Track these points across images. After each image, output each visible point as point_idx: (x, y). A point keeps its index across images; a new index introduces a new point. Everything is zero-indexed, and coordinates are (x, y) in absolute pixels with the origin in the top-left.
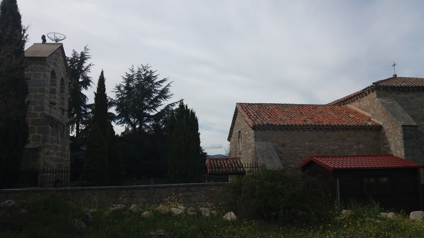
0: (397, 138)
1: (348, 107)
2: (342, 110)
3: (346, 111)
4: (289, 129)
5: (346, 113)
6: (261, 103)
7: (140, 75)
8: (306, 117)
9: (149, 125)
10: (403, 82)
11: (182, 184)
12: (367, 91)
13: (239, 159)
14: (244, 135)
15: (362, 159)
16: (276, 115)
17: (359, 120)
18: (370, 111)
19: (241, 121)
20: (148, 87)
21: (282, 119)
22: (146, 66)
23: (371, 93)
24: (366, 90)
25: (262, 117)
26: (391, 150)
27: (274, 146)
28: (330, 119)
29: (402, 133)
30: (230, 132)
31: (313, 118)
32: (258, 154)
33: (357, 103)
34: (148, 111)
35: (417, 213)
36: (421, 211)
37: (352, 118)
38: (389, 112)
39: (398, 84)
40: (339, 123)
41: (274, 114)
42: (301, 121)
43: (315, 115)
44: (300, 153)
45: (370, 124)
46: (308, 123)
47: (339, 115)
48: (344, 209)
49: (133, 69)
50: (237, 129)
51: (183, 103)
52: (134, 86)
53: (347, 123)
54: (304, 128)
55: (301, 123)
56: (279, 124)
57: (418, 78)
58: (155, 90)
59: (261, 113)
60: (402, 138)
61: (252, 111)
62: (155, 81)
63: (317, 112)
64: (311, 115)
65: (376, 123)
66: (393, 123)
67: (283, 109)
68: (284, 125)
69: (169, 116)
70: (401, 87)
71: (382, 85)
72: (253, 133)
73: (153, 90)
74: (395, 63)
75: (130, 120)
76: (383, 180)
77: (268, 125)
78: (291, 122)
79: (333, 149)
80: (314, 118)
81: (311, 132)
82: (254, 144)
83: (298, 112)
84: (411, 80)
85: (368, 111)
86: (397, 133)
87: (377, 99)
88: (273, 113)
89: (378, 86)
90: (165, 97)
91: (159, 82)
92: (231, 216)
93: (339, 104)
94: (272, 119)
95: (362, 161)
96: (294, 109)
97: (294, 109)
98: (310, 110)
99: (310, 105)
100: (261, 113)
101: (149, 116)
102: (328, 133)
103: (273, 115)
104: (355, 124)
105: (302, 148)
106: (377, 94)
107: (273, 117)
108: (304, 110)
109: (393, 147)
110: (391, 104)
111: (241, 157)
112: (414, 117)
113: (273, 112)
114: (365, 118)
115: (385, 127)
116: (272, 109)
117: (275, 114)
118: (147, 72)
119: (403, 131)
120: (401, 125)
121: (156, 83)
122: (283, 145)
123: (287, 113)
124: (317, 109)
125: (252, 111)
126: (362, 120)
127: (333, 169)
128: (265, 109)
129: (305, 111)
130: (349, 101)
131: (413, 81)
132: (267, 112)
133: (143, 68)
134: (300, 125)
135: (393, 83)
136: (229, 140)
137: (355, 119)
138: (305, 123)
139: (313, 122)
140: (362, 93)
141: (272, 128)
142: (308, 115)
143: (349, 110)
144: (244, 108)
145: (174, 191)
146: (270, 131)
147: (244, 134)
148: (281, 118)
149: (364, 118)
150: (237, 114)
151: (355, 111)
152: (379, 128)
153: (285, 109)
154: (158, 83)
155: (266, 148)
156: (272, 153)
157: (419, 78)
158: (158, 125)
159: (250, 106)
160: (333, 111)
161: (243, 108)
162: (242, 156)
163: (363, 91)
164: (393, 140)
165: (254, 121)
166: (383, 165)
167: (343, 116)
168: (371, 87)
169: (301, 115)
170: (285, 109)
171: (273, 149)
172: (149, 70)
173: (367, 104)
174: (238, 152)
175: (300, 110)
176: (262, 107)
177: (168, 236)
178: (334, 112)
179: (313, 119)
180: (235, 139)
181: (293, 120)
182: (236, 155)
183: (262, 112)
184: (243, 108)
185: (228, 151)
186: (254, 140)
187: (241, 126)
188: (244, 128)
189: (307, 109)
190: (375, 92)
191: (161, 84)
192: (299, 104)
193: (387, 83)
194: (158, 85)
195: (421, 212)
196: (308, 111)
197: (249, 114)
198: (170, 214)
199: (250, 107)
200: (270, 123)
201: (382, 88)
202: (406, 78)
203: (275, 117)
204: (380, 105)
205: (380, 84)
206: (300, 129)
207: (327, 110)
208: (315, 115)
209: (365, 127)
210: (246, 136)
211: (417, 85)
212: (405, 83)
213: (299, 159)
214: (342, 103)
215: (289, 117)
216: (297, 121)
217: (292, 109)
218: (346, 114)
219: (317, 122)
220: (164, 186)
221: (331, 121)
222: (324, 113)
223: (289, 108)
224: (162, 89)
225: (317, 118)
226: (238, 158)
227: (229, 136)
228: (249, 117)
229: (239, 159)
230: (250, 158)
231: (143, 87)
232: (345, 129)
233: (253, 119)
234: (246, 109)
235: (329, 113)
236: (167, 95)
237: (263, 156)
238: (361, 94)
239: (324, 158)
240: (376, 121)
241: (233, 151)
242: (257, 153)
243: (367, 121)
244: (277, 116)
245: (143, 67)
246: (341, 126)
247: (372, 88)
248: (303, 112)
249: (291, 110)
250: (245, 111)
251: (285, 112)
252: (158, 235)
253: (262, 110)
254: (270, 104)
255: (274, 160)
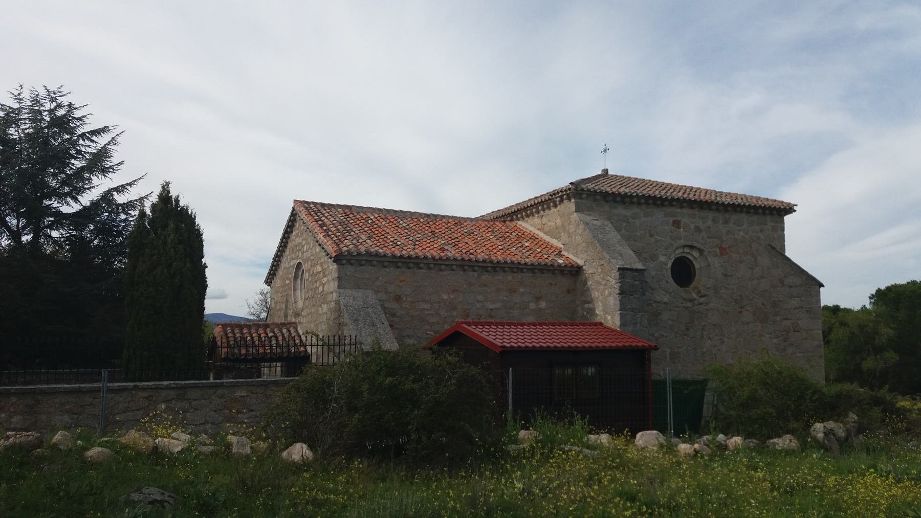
0: (608, 291)
1: (519, 227)
2: (508, 232)
3: (515, 234)
4: (411, 265)
5: (516, 239)
6: (351, 205)
7: (40, 112)
8: (443, 242)
9: (59, 238)
10: (621, 184)
11: (165, 383)
12: (558, 197)
13: (294, 325)
14: (311, 273)
15: (511, 329)
16: (383, 233)
17: (541, 254)
18: (560, 236)
19: (304, 242)
20: (61, 142)
21: (396, 243)
22: (55, 89)
23: (564, 201)
24: (557, 196)
25: (355, 236)
26: (597, 314)
27: (379, 300)
28: (488, 249)
29: (618, 283)
30: (273, 265)
31: (457, 245)
32: (344, 316)
33: (536, 220)
34: (56, 202)
35: (647, 434)
36: (653, 430)
37: (528, 248)
38: (596, 242)
39: (614, 187)
40: (506, 257)
41: (378, 231)
42: (435, 249)
43: (460, 238)
44: (429, 314)
45: (561, 261)
46: (447, 255)
47: (505, 241)
48: (521, 429)
49: (19, 94)
50: (293, 260)
51: (169, 192)
52: (20, 138)
53: (521, 258)
54: (441, 264)
55: (435, 254)
56: (392, 254)
57: (644, 180)
58: (79, 152)
59: (352, 227)
60: (618, 291)
61: (331, 221)
62: (79, 131)
63: (462, 232)
64: (453, 237)
65: (571, 261)
66: (602, 262)
67: (396, 220)
68: (401, 257)
69: (111, 217)
70: (619, 194)
71: (587, 187)
72: (334, 269)
73: (73, 152)
74: (608, 147)
75: (7, 222)
76: (587, 371)
77: (368, 253)
78: (415, 250)
79: (491, 309)
80: (459, 245)
81: (453, 272)
82: (335, 295)
83: (427, 230)
84: (633, 181)
85: (558, 236)
86: (608, 282)
87: (575, 214)
88: (375, 228)
89: (579, 189)
90: (105, 171)
91: (89, 134)
92: (299, 452)
93: (502, 219)
94: (376, 242)
95: (511, 335)
96: (419, 222)
97: (419, 222)
98: (450, 226)
99: (448, 216)
100: (352, 227)
101: (59, 215)
102: (485, 277)
103: (376, 232)
104: (534, 260)
105: (434, 304)
106: (577, 204)
107: (377, 238)
108: (437, 227)
109: (601, 308)
110: (600, 226)
111: (300, 323)
112: (638, 253)
113: (375, 226)
114: (551, 251)
115: (587, 270)
116: (374, 220)
117: (380, 230)
118: (60, 106)
119: (619, 279)
120: (618, 267)
121: (83, 136)
122: (398, 299)
123: (406, 231)
124: (462, 226)
125: (331, 221)
126: (546, 253)
127: (500, 350)
128: (358, 219)
129: (440, 230)
130: (522, 214)
131: (638, 185)
132: (364, 226)
133: (47, 95)
134: (433, 258)
135: (605, 186)
136: (268, 281)
137: (534, 252)
138: (442, 254)
139: (458, 253)
140: (548, 200)
141: (377, 261)
142: (447, 237)
143: (521, 231)
144: (313, 213)
145: (145, 398)
146: (373, 268)
147: (311, 271)
148: (395, 241)
149: (550, 250)
150: (293, 226)
151: (532, 234)
152: (575, 271)
153: (401, 222)
154: (87, 135)
155: (362, 304)
156: (375, 314)
157: (647, 180)
158: (81, 238)
159: (325, 210)
160: (492, 231)
161: (310, 213)
162: (301, 319)
163: (550, 197)
164: (600, 294)
165: (338, 245)
166: (561, 343)
167: (512, 243)
168: (566, 190)
169: (432, 236)
170: (401, 222)
171: (378, 307)
172: (65, 101)
173: (556, 223)
174: (292, 311)
175: (430, 227)
176: (353, 214)
177: (170, 502)
178: (494, 235)
179: (457, 247)
180: (285, 281)
181: (418, 246)
182: (286, 316)
183: (354, 224)
184: (310, 213)
185: (256, 307)
186: (337, 286)
187: (303, 253)
188: (312, 258)
189: (444, 224)
190: (573, 200)
191: (94, 138)
192: (428, 213)
193: (594, 185)
194: (86, 141)
195: (655, 432)
196: (447, 230)
197: (325, 228)
198: (157, 453)
199: (325, 212)
200: (374, 250)
201: (587, 194)
202: (623, 177)
203: (382, 237)
204: (582, 227)
205: (584, 186)
206: (432, 266)
207: (481, 230)
208: (460, 238)
209: (552, 268)
210: (316, 275)
211: (646, 194)
212: (625, 187)
213: (427, 327)
214: (508, 217)
215: (411, 238)
216: (428, 249)
217: (415, 224)
218: (517, 240)
219: (466, 253)
220: (118, 386)
221: (491, 252)
222: (476, 235)
223: (409, 220)
224: (95, 151)
225: (464, 244)
226: (292, 325)
227: (269, 274)
228: (325, 234)
229: (294, 325)
230: (323, 324)
231: (46, 142)
232: (515, 270)
233: (336, 238)
234: (318, 216)
235: (485, 237)
236: (108, 164)
237: (356, 320)
238: (546, 202)
239: (481, 326)
240: (571, 257)
241: (278, 307)
242: (342, 314)
243: (555, 255)
244: (386, 235)
245: (49, 92)
246: (509, 263)
247: (569, 192)
248: (437, 231)
249: (412, 225)
250: (317, 221)
251: (401, 228)
252: (150, 500)
253: (352, 221)
254: (369, 208)
255: (379, 329)
